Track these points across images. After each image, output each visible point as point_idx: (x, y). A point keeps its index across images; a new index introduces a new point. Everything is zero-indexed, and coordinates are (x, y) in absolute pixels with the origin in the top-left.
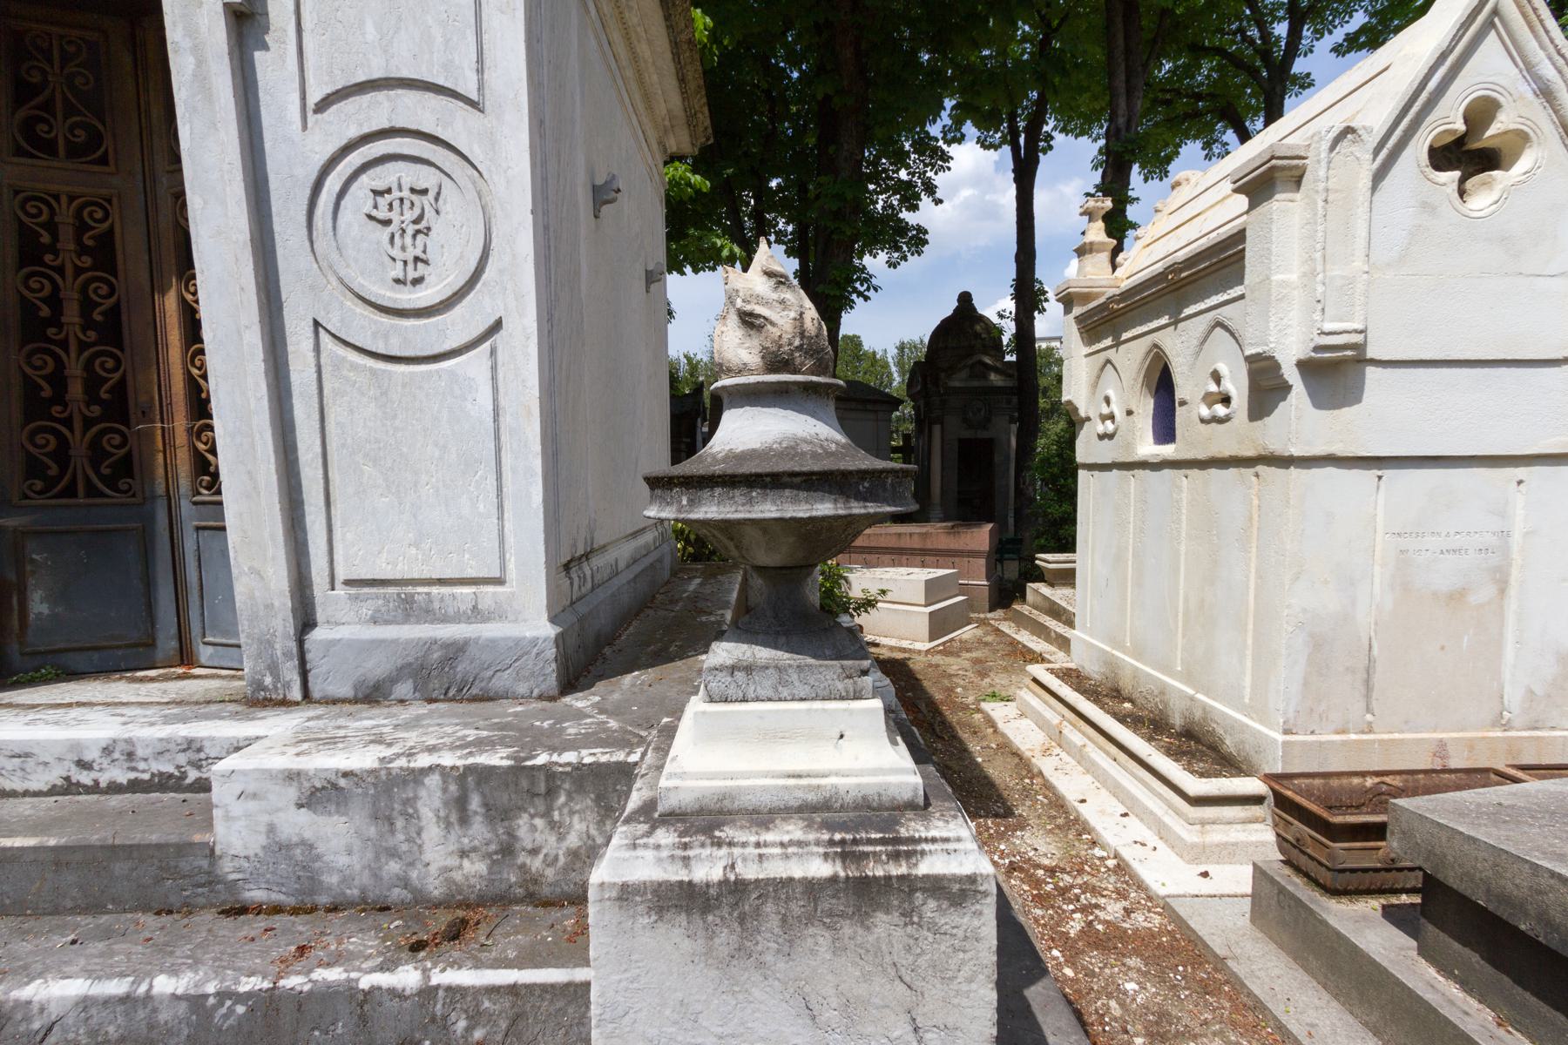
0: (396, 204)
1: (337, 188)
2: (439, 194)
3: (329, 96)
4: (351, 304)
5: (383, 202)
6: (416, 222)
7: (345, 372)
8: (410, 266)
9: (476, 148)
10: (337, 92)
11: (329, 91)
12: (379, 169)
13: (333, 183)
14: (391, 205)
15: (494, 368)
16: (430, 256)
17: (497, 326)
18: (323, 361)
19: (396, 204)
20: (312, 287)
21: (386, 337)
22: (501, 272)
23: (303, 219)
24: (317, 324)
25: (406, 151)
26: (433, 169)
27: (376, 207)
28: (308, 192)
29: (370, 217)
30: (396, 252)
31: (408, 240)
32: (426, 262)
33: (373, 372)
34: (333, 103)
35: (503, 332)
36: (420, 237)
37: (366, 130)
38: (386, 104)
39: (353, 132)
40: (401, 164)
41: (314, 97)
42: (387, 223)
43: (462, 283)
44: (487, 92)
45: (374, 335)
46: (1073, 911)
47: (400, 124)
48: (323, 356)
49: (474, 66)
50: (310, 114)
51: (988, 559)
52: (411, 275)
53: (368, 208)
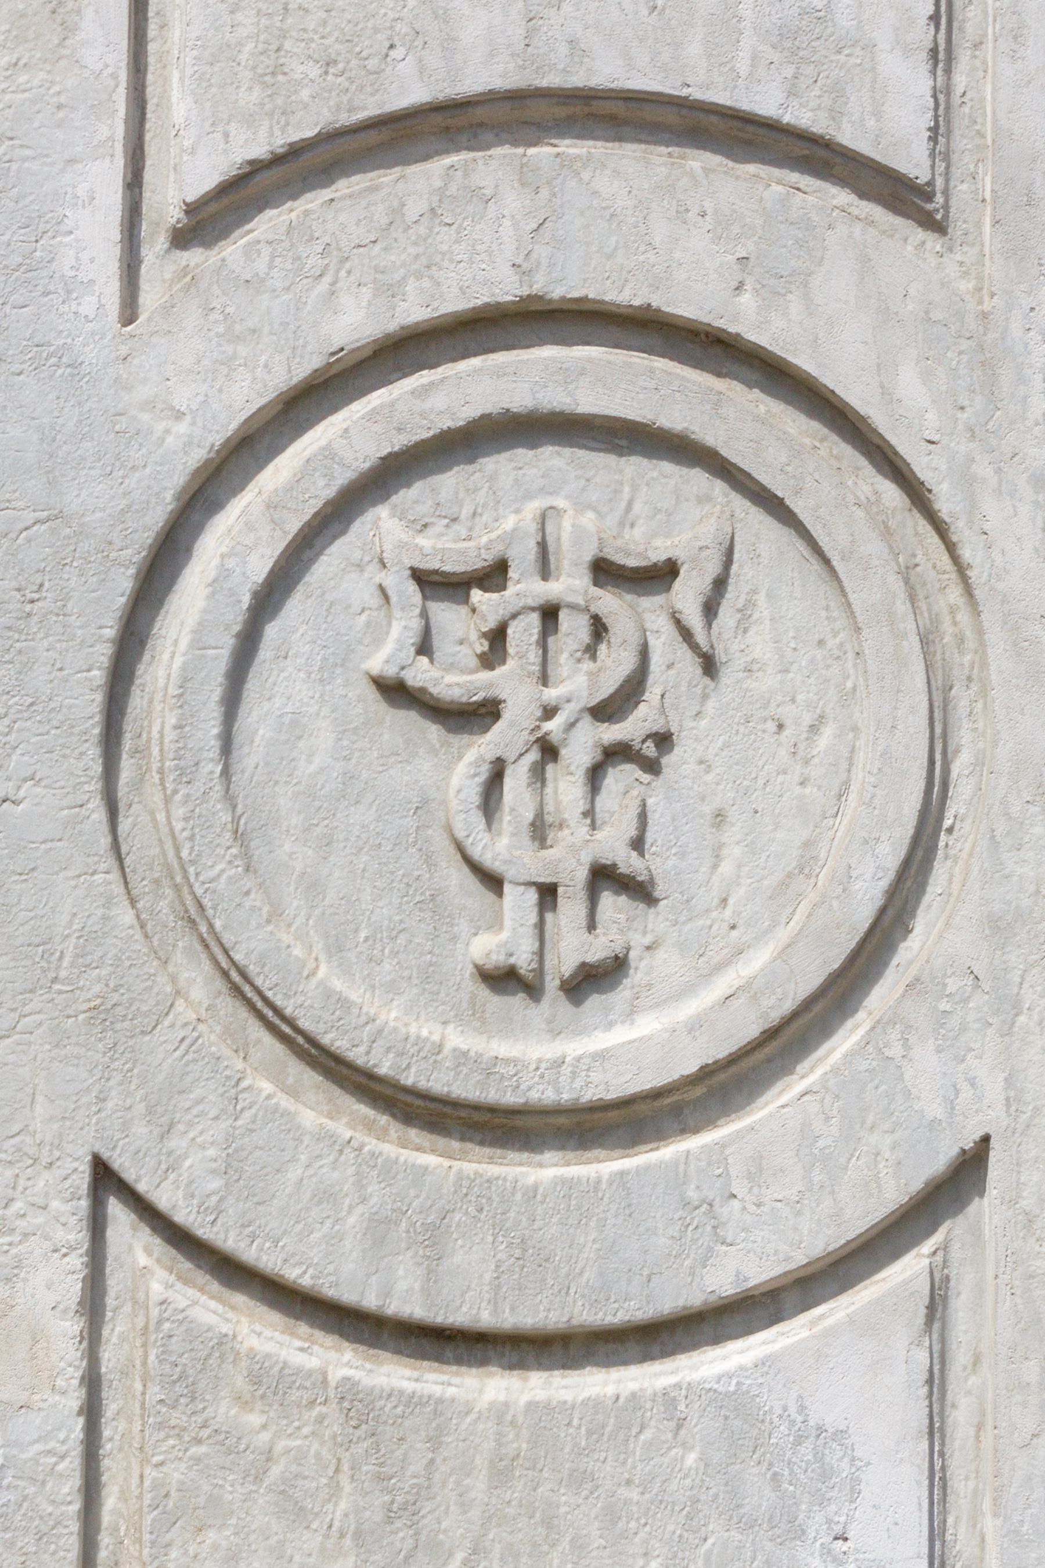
0: (523, 634)
1: (259, 567)
2: (720, 584)
3: (256, 168)
4: (276, 1086)
5: (459, 625)
6: (605, 711)
7: (223, 1411)
8: (571, 909)
9: (912, 388)
10: (295, 151)
11: (259, 151)
12: (449, 482)
13: (237, 543)
14: (498, 637)
15: (936, 1383)
16: (658, 864)
17: (968, 1171)
18: (109, 1358)
19: (523, 634)
20: (101, 1015)
21: (433, 1240)
22: (998, 928)
23: (88, 705)
24: (104, 1178)
25: (587, 401)
26: (698, 479)
27: (424, 648)
28: (123, 584)
29: (395, 691)
30: (502, 847)
31: (567, 788)
32: (640, 890)
33: (357, 1405)
34: (262, 203)
35: (988, 1208)
36: (621, 777)
37: (414, 310)
38: (513, 202)
39: (354, 322)
40: (553, 459)
41: (189, 168)
42: (476, 715)
43: (808, 979)
44: (962, 142)
45: (378, 1231)
46: (320, 710)
47: (568, 282)
48: (117, 1329)
49: (922, 35)
50: (154, 248)
51: (434, 598)
52: (572, 946)
53: (389, 653)
